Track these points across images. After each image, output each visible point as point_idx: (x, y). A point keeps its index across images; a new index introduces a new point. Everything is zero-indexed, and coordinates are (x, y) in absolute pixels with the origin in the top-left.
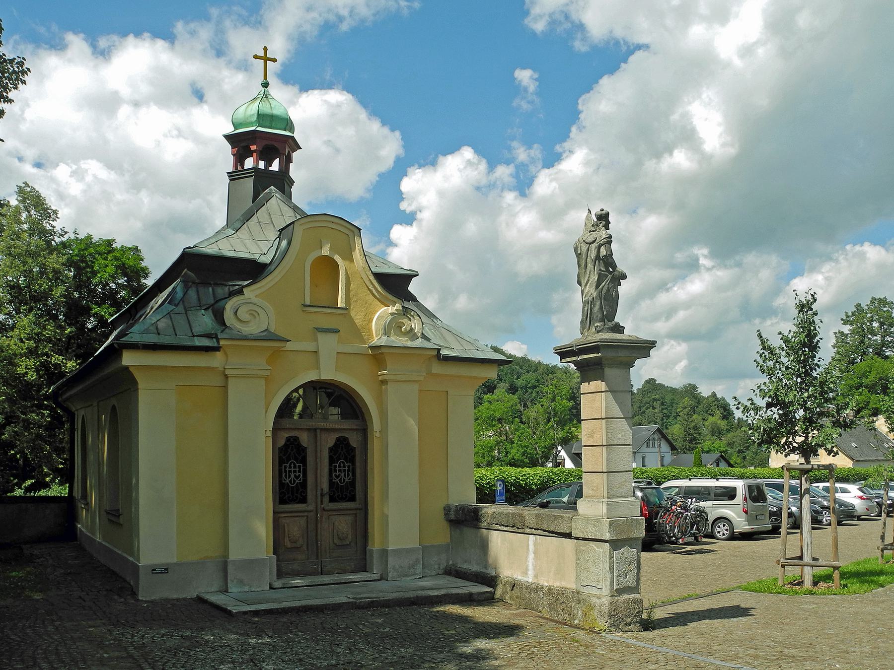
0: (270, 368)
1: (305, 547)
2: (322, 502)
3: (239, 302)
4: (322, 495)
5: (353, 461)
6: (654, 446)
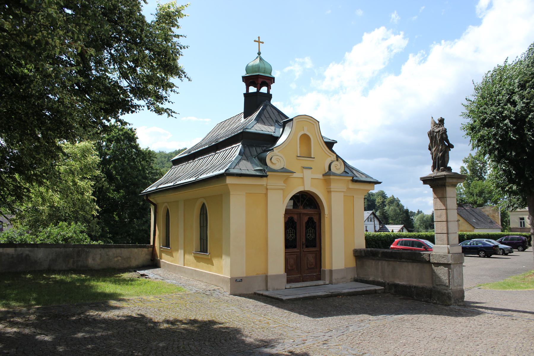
0: (285, 185)
1: (296, 269)
2: (303, 248)
4: (303, 244)
5: (315, 228)
6: (371, 221)
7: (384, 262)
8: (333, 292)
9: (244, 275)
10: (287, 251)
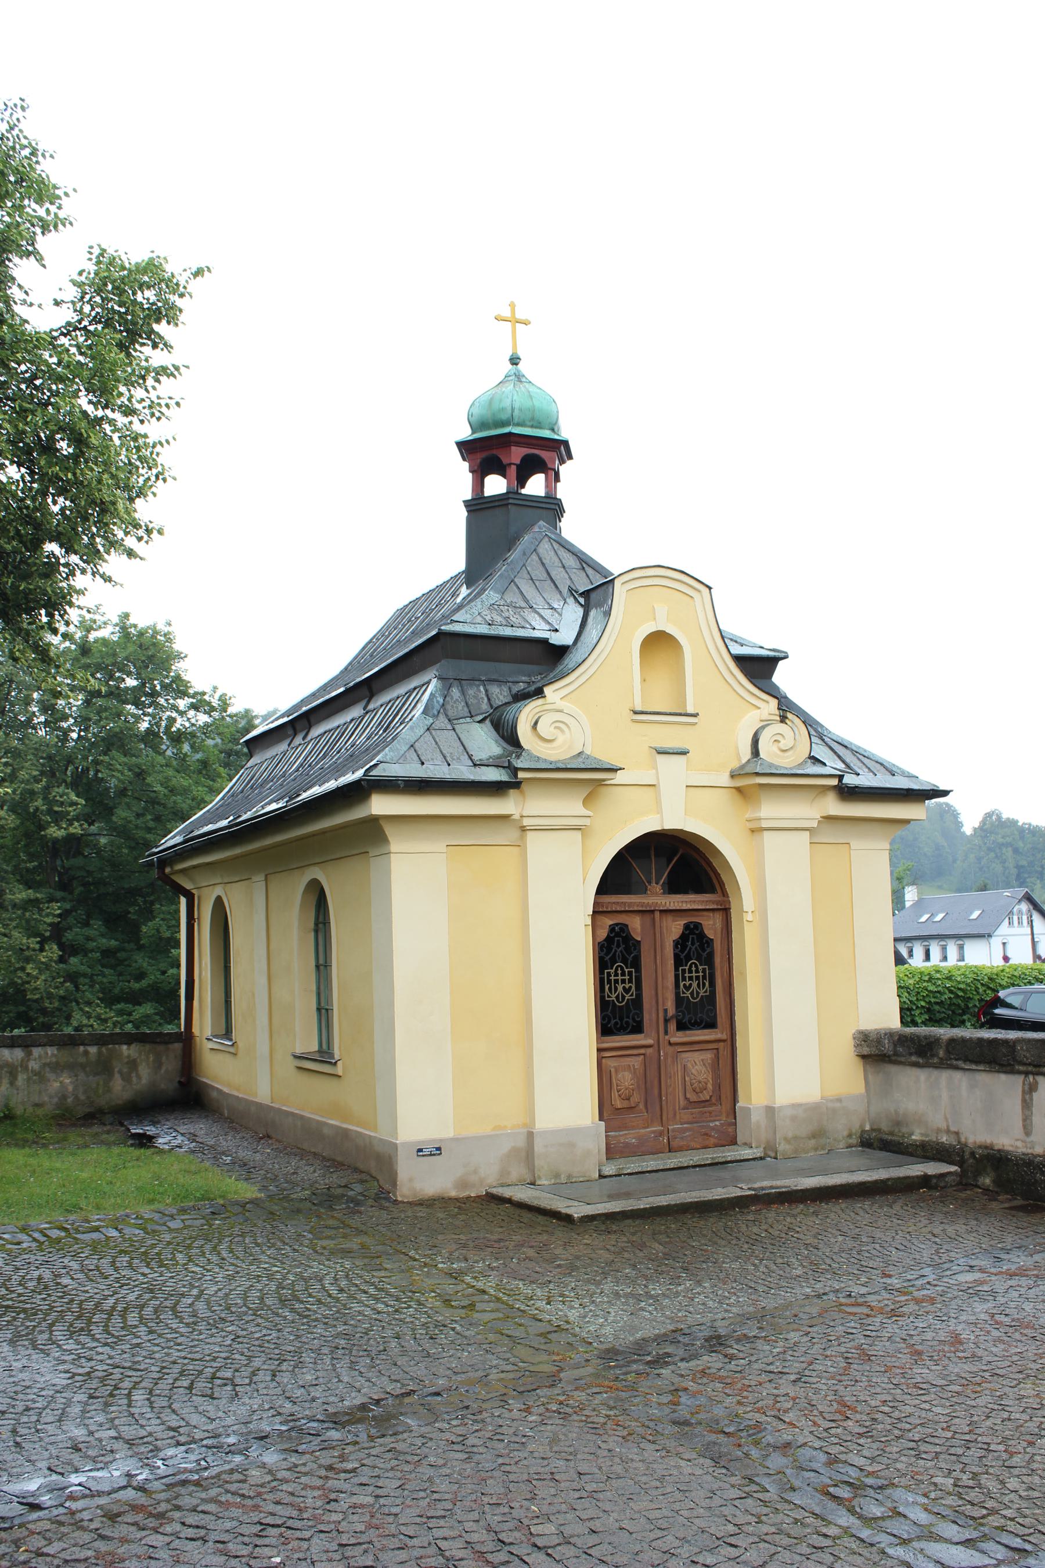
0: (588, 813)
1: (641, 1106)
2: (666, 1033)
4: (666, 1021)
5: (709, 961)
6: (1020, 922)
7: (957, 1075)
8: (763, 1188)
9: (449, 1133)
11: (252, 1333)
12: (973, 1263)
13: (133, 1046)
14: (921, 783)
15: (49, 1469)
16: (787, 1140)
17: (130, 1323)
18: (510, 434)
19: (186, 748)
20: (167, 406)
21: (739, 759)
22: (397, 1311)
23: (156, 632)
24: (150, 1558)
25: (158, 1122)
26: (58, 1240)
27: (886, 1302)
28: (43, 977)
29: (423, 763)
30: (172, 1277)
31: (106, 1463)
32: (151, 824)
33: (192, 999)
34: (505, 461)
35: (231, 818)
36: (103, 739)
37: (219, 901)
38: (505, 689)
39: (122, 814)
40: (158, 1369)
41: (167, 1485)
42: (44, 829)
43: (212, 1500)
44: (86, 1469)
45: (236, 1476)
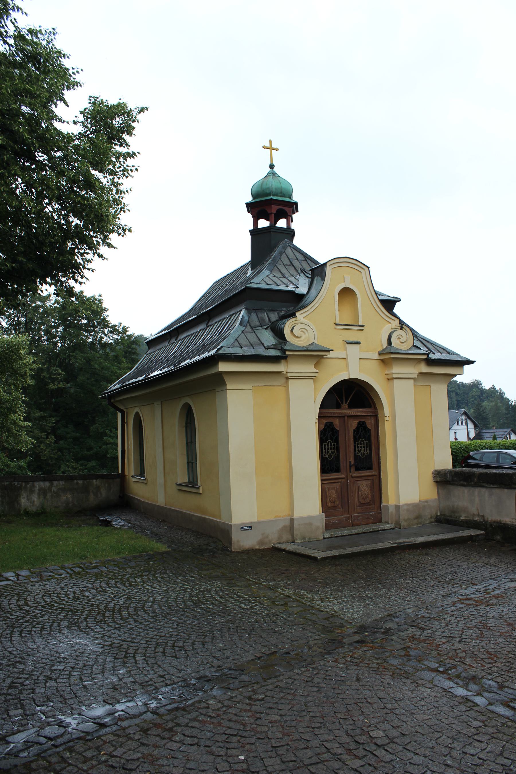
1: (340, 506)
2: (350, 472)
3: (293, 323)
4: (350, 467)
6: (462, 424)
7: (483, 490)
9: (255, 519)
10: (324, 478)
11: (185, 621)
12: (511, 577)
13: (98, 480)
14: (461, 357)
15: (104, 701)
16: (405, 520)
17: (124, 617)
18: (271, 199)
19: (108, 350)
20: (131, 170)
21: (382, 346)
22: (251, 608)
23: (95, 299)
24: (173, 757)
25: (112, 514)
26: (79, 573)
27: (481, 598)
28: (48, 450)
29: (242, 348)
30: (137, 592)
31: (133, 697)
32: (94, 383)
33: (125, 459)
34: (269, 212)
35: (144, 376)
36: (72, 346)
37: (137, 414)
38: (276, 313)
39: (81, 378)
40: (145, 642)
41: (169, 710)
42: (47, 385)
43: (195, 720)
44: (123, 701)
45: (203, 705)
